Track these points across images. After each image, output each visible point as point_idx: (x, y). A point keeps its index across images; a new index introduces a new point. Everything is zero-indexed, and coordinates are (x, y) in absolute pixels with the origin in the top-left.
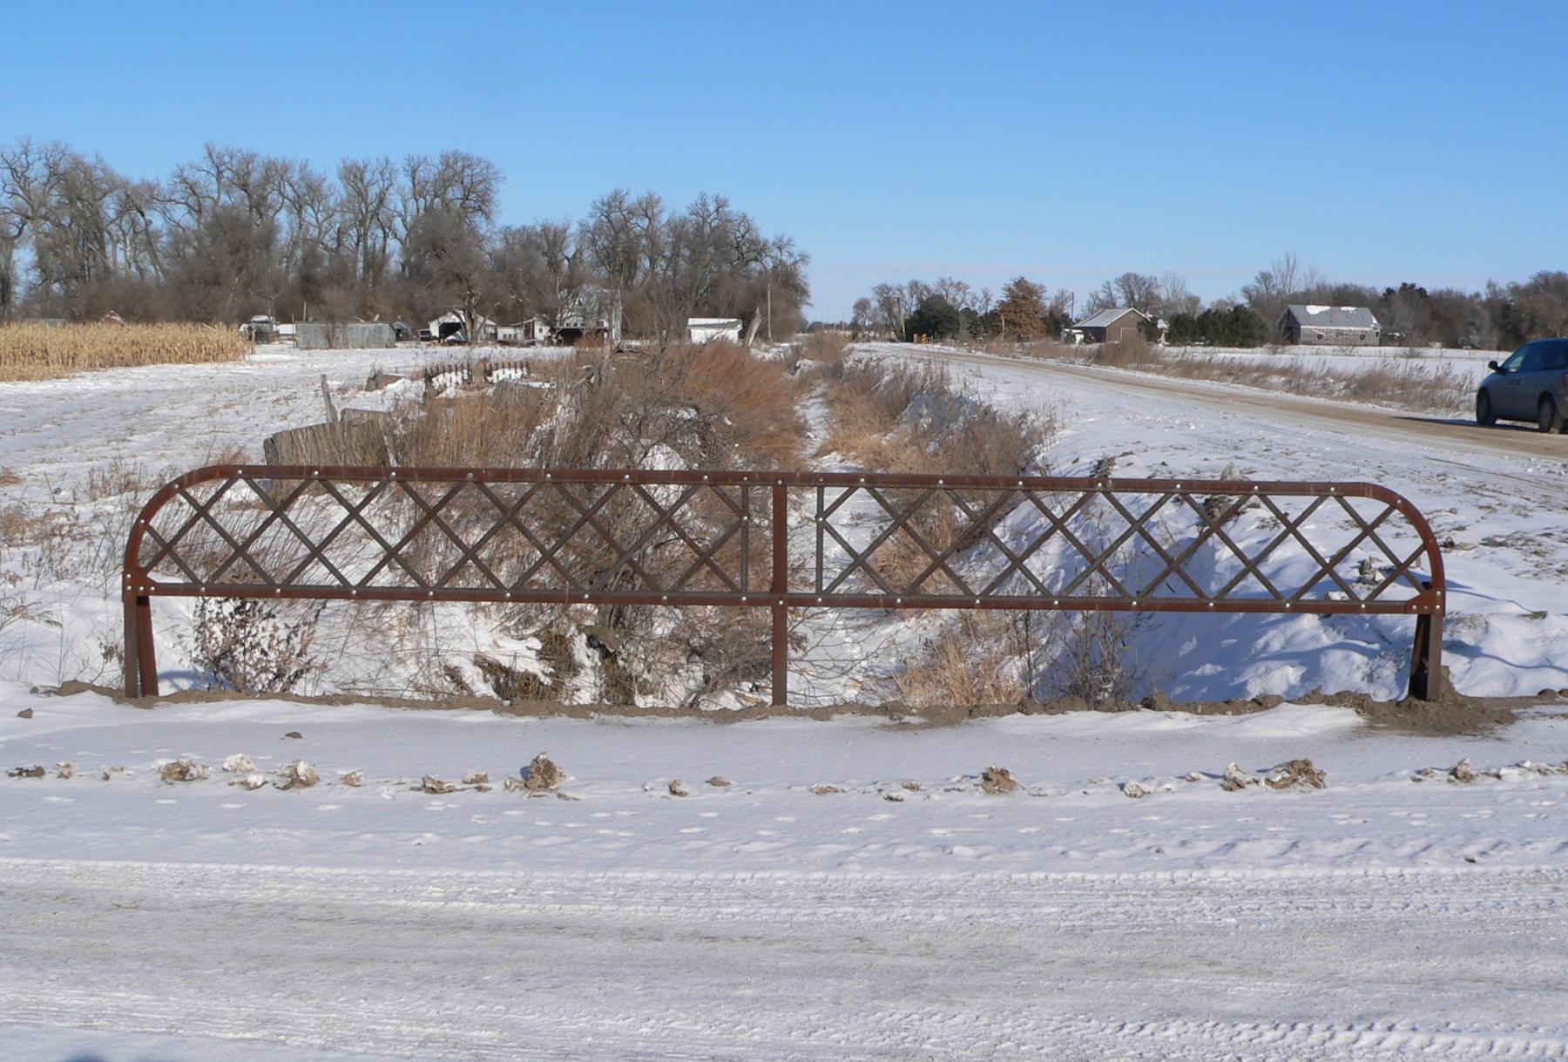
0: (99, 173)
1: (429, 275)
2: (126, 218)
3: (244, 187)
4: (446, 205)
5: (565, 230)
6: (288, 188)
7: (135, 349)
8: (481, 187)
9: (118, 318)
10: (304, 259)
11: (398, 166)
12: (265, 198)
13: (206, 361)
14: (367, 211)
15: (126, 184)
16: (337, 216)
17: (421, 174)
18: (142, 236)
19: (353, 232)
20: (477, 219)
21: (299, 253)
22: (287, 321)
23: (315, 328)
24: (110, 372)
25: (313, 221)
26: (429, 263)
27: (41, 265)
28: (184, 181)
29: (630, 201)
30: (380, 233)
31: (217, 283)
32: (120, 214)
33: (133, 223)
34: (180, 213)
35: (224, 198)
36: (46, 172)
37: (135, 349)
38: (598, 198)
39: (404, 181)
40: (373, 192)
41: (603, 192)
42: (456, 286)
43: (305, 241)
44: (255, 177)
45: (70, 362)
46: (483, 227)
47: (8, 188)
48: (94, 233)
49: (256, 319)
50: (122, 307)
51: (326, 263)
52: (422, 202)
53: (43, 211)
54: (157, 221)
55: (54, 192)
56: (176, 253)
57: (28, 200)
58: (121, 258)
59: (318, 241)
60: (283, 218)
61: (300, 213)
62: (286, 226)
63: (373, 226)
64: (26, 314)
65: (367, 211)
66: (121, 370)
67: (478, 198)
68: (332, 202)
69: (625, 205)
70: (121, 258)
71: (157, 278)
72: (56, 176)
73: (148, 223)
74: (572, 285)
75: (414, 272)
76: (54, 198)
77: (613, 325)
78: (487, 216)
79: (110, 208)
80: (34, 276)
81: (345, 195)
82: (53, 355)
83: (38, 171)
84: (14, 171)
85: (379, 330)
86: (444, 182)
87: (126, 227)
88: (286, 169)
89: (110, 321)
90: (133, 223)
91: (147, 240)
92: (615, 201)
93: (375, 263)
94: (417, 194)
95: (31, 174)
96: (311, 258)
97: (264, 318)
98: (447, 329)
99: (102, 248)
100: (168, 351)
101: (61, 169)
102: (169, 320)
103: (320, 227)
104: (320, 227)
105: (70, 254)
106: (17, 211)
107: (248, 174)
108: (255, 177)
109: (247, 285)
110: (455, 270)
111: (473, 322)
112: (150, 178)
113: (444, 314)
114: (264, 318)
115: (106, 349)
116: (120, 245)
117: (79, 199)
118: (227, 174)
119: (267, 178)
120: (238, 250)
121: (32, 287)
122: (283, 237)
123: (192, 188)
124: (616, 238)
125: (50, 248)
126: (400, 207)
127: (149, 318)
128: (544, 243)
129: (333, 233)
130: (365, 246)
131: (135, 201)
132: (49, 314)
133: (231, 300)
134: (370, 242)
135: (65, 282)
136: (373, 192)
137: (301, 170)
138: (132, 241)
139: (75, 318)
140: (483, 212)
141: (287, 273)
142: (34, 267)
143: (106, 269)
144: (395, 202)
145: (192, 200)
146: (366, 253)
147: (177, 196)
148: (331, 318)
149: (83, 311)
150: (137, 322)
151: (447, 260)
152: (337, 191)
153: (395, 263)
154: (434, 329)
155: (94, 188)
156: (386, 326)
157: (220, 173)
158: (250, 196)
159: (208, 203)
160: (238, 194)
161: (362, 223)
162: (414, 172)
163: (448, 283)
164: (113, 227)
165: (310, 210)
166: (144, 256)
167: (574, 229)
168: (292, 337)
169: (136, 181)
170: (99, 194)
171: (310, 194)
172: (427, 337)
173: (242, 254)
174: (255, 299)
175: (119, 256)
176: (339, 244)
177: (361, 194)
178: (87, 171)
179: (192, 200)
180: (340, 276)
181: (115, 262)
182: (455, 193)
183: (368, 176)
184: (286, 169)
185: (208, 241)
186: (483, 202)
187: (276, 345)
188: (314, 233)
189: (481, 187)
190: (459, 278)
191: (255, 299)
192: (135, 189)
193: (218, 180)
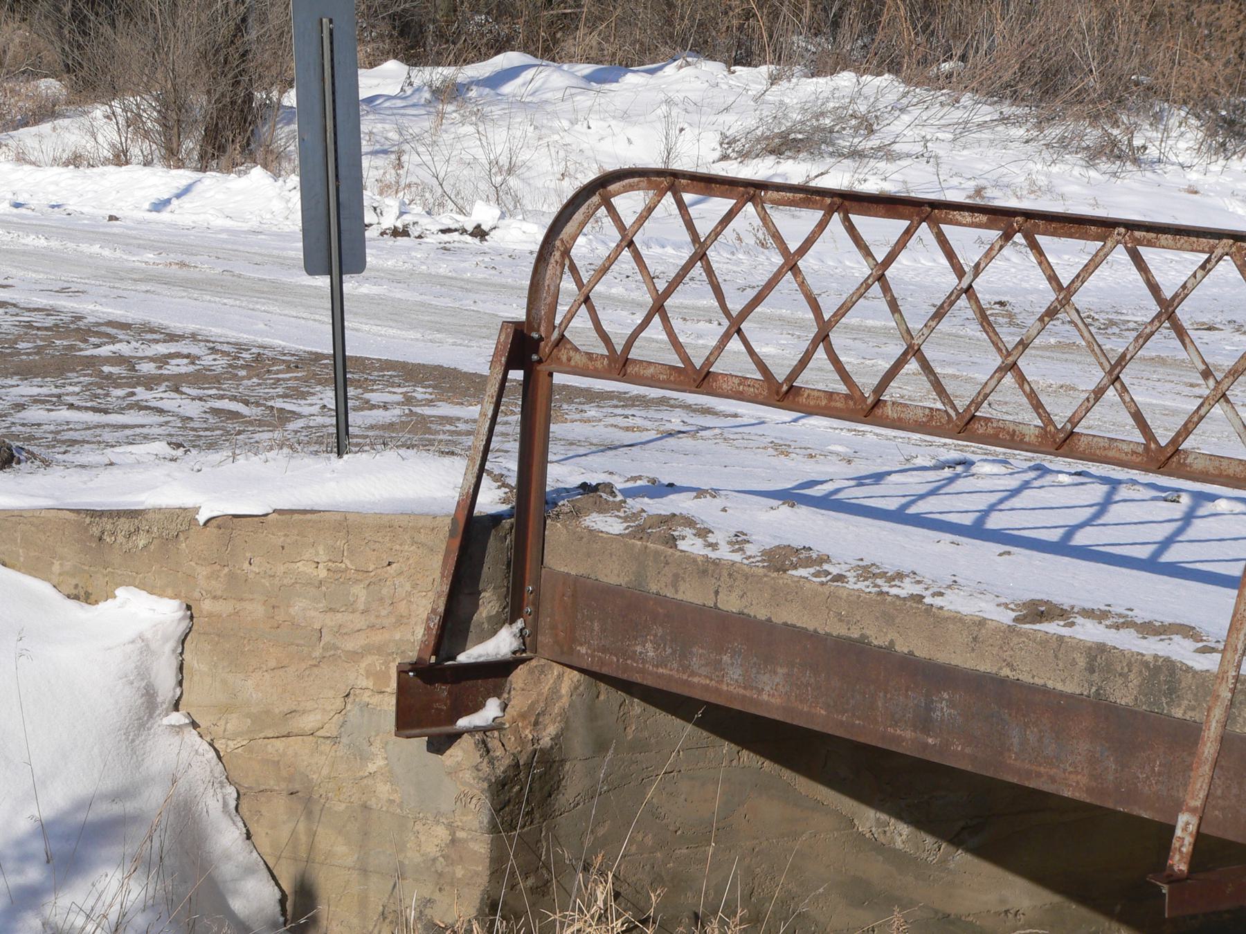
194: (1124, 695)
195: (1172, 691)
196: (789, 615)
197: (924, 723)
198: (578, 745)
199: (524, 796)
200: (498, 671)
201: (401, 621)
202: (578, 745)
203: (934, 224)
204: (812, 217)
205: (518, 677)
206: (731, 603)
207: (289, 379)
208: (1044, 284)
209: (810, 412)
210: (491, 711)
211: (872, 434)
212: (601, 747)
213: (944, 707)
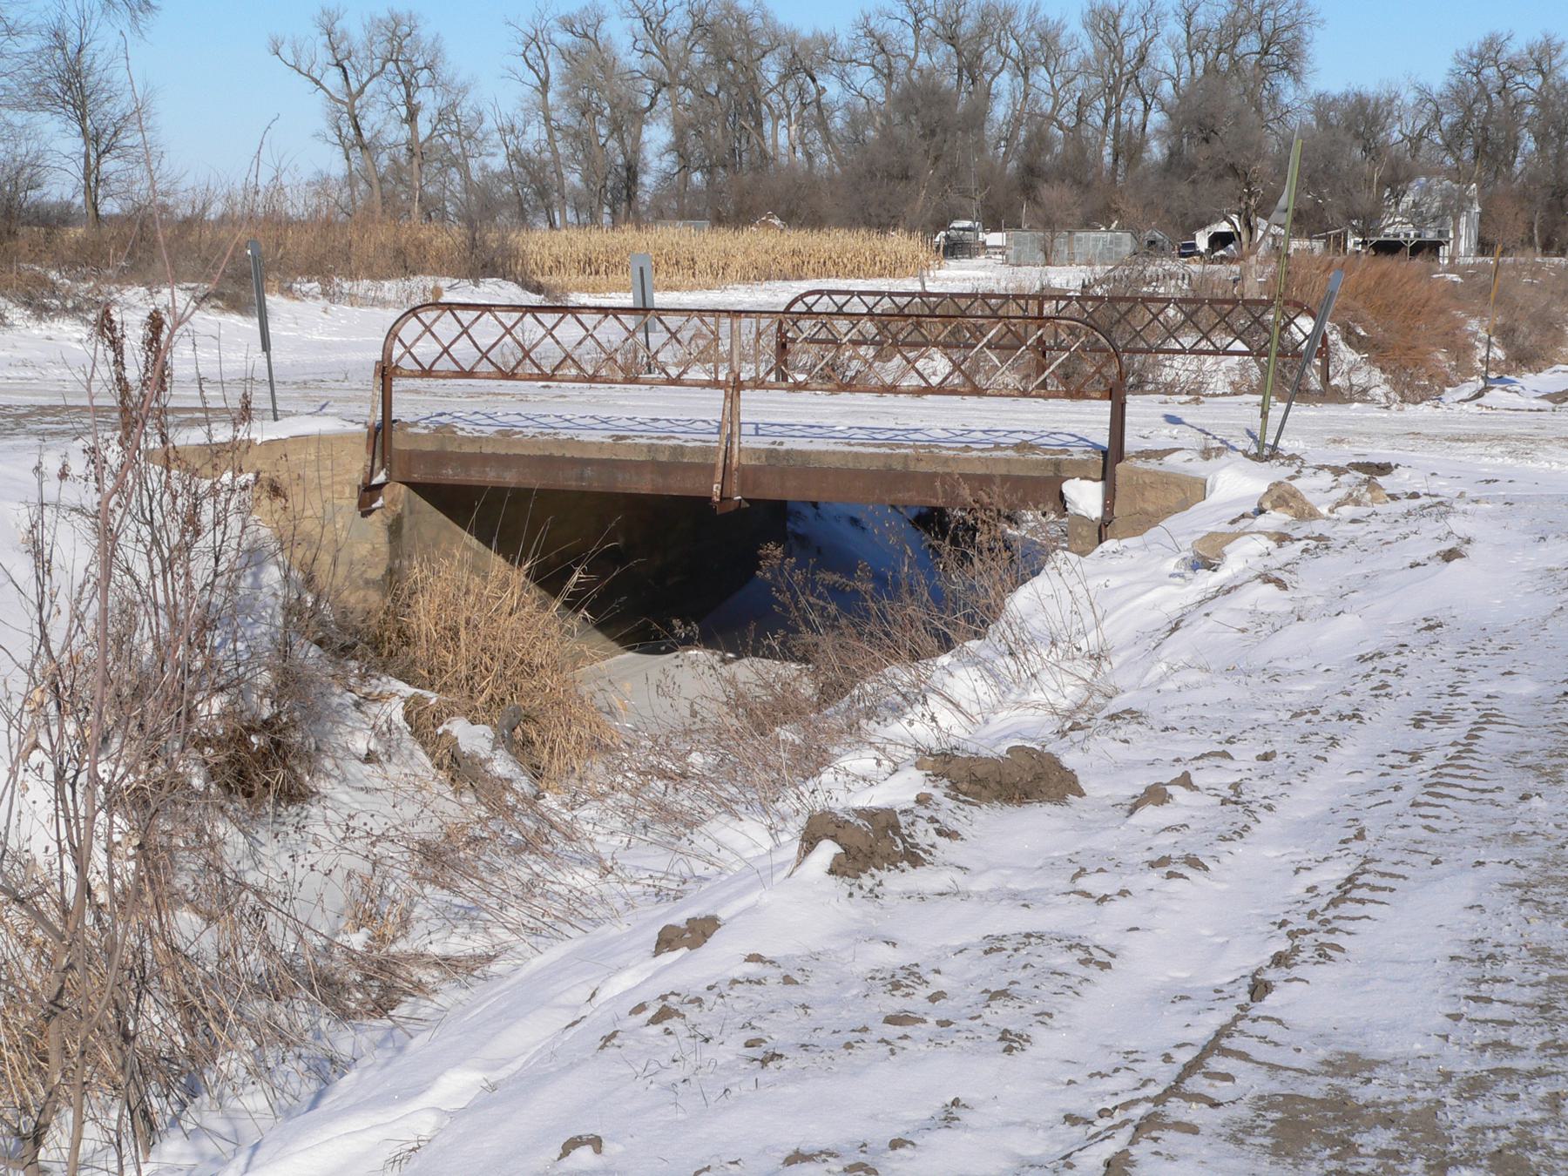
0: (757, 22)
1: (1192, 168)
2: (791, 85)
3: (952, 39)
4: (1235, 63)
5: (1391, 101)
6: (1013, 43)
7: (796, 260)
8: (1287, 35)
9: (777, 222)
10: (1028, 142)
11: (1167, 8)
12: (979, 57)
13: (880, 276)
14: (1121, 72)
15: (792, 38)
16: (1080, 81)
17: (1200, 19)
18: (813, 110)
19: (1101, 104)
20: (1281, 82)
21: (1023, 134)
22: (996, 229)
23: (1029, 237)
24: (766, 285)
25: (1046, 86)
26: (1191, 150)
27: (679, 147)
28: (871, 33)
29: (1515, 48)
30: (1139, 104)
31: (905, 177)
32: (784, 78)
33: (801, 91)
34: (863, 77)
35: (923, 59)
36: (688, 22)
37: (796, 260)
38: (1463, 46)
39: (1174, 28)
40: (1131, 45)
41: (1473, 38)
42: (1230, 182)
43: (1031, 115)
44: (968, 26)
45: (720, 273)
46: (1289, 93)
47: (639, 45)
48: (747, 105)
49: (957, 224)
50: (783, 207)
51: (1058, 148)
52: (1200, 59)
53: (683, 75)
54: (833, 90)
55: (697, 48)
56: (857, 140)
57: (665, 60)
58: (783, 139)
59: (1052, 118)
60: (1004, 83)
61: (1025, 77)
62: (1006, 98)
63: (1129, 94)
64: (660, 214)
65: (1121, 72)
66: (778, 284)
67: (1285, 53)
68: (1073, 61)
69: (1503, 57)
70: (783, 139)
71: (830, 169)
72: (702, 28)
73: (821, 91)
74: (1396, 181)
75: (1176, 163)
76: (698, 57)
77: (1462, 242)
78: (1297, 78)
79: (771, 70)
80: (668, 162)
81: (1090, 51)
82: (701, 265)
83: (678, 21)
84: (647, 21)
85: (1117, 242)
86: (1232, 32)
87: (791, 96)
88: (1009, 14)
89: (766, 224)
90: (801, 91)
91: (818, 114)
92: (1490, 50)
93: (1129, 147)
94: (1195, 44)
95: (670, 25)
96: (1040, 141)
97: (967, 224)
98: (1219, 240)
99: (759, 125)
100: (835, 263)
101: (708, 18)
102: (839, 225)
103: (1056, 97)
104: (1056, 97)
105: (716, 133)
106: (650, 74)
107: (958, 22)
108: (968, 26)
109: (943, 180)
110: (1228, 160)
111: (1251, 230)
112: (825, 29)
113: (1216, 221)
114: (967, 224)
115: (763, 259)
116: (782, 122)
117: (731, 59)
118: (930, 23)
119: (984, 29)
120: (933, 133)
121: (667, 177)
122: (1000, 111)
123: (880, 44)
124: (1469, 110)
125: (692, 126)
126: (1171, 67)
127: (816, 221)
128: (1361, 119)
129: (1072, 106)
130: (1118, 124)
131: (803, 61)
132: (686, 215)
133: (921, 202)
134: (1124, 117)
135: (710, 171)
136: (1131, 45)
137: (1029, 17)
138: (799, 115)
139: (719, 220)
140: (1291, 71)
141: (1005, 162)
142: (669, 150)
143: (763, 154)
144: (1164, 58)
145: (880, 59)
146: (1116, 134)
147: (860, 55)
148: (1049, 224)
149: (732, 211)
150: (801, 226)
151: (1218, 146)
152: (1080, 43)
153: (1156, 151)
154: (1202, 242)
155: (750, 44)
156: (1127, 237)
157: (918, 21)
158: (959, 54)
159: (901, 64)
160: (943, 51)
161: (1113, 90)
162: (1190, 16)
163: (1219, 177)
164: (774, 98)
165: (1043, 71)
166: (815, 135)
167: (1409, 97)
168: (1001, 250)
169: (806, 32)
170: (757, 52)
171: (1048, 45)
172: (1189, 251)
173: (937, 138)
174: (954, 199)
175: (781, 137)
176: (1080, 120)
177: (1113, 48)
178: (741, 19)
179: (880, 59)
180: (1076, 170)
181: (775, 146)
182: (1249, 45)
183: (1124, 23)
184: (1009, 14)
185: (897, 118)
186: (1290, 56)
187: (981, 260)
188: (1047, 105)
189: (1287, 35)
190: (1233, 169)
191: (954, 199)
192: (805, 44)
193: (917, 30)
194: (663, 458)
195: (682, 455)
196: (518, 451)
197: (582, 478)
198: (406, 513)
199: (395, 529)
200: (381, 486)
201: (349, 471)
202: (406, 513)
203: (573, 314)
204: (516, 315)
205: (386, 489)
206: (488, 450)
207: (1511, 422)
208: (669, 347)
209: (437, 377)
210: (380, 502)
211: (432, 381)
212: (411, 512)
213: (588, 472)
